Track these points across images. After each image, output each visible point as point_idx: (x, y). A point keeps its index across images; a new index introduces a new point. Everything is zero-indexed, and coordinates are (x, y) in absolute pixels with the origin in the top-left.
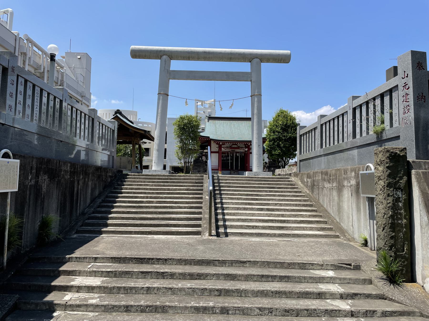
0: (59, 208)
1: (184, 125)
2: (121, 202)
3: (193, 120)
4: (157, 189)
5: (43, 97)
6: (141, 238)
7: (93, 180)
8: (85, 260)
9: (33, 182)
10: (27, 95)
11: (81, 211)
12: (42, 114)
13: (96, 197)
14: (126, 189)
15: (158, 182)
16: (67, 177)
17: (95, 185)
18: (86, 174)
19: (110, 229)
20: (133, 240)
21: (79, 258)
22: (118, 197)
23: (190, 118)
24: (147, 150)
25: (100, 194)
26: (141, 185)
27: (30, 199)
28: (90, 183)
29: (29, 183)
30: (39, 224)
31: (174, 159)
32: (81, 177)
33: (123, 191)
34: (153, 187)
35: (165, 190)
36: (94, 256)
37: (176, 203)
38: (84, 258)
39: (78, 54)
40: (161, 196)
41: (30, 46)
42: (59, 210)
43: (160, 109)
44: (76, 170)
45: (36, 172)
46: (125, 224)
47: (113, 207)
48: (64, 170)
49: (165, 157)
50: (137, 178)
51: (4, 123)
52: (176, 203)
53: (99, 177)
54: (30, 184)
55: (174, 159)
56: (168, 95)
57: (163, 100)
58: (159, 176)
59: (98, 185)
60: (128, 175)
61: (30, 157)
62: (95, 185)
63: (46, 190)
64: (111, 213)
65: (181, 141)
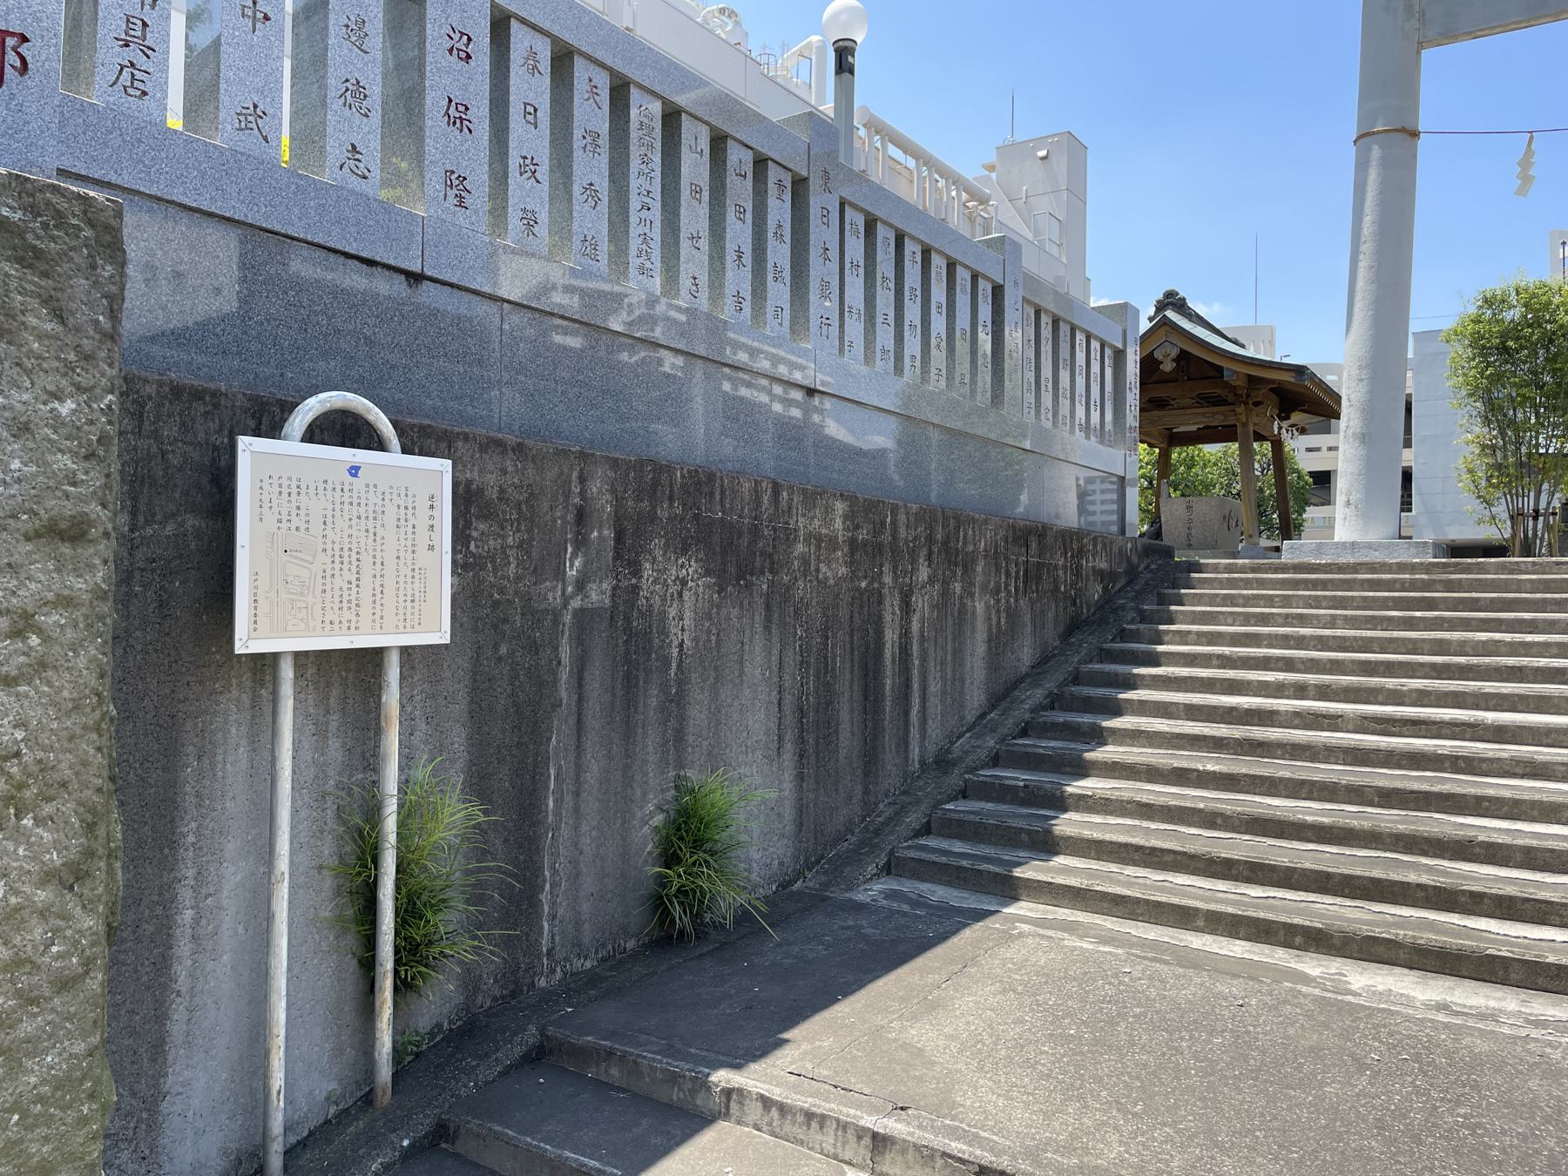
0: (789, 736)
1: (1504, 336)
2: (1144, 708)
3: (1556, 300)
4: (1366, 645)
5: (685, 150)
6: (1250, 971)
7: (998, 591)
8: (814, 1135)
9: (599, 594)
10: (577, 134)
11: (931, 748)
12: (685, 246)
13: (1021, 680)
14: (1183, 637)
15: (1367, 604)
16: (835, 569)
17: (1013, 615)
18: (952, 558)
19: (1064, 869)
20: (1191, 987)
21: (783, 1109)
22: (1131, 683)
23: (1534, 296)
24: (1323, 479)
25: (1043, 662)
26: (1264, 620)
27: (580, 679)
28: (980, 607)
29: (566, 600)
30: (659, 819)
31: (1459, 506)
32: (924, 573)
33: (1161, 648)
34: (1339, 632)
35: (1415, 647)
36: (869, 1121)
37: (1500, 734)
38: (809, 1116)
39: (1039, 142)
40: (1391, 683)
41: (878, 145)
42: (789, 746)
43: (1368, 220)
44: (886, 537)
45: (619, 538)
46: (1153, 850)
47: (1099, 737)
48: (809, 537)
49: (1406, 505)
50: (1248, 584)
51: (415, 267)
52: (1500, 734)
53: (1032, 576)
54: (576, 603)
55: (1459, 506)
56: (1415, 134)
57: (1384, 164)
58: (1371, 567)
59: (1028, 618)
60: (1199, 568)
61: (564, 453)
62: (1013, 615)
63: (696, 640)
64: (1082, 769)
65: (1493, 412)
